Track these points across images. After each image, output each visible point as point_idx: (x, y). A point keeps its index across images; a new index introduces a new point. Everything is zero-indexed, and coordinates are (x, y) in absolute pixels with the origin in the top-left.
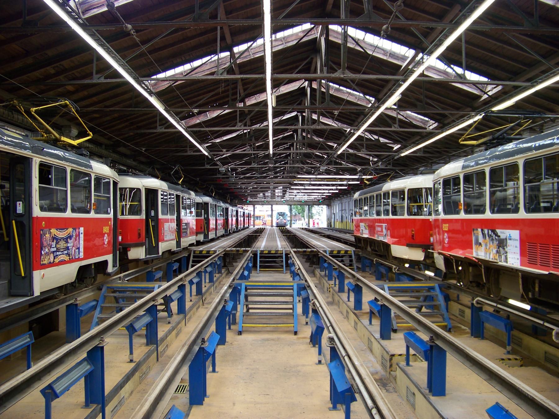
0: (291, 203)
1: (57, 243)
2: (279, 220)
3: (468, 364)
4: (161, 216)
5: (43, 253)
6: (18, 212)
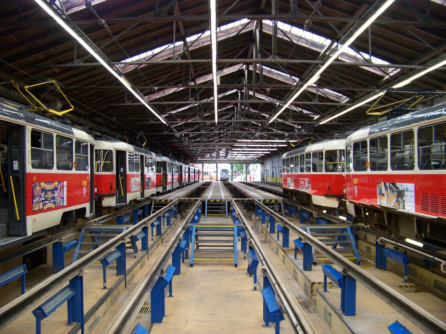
0: (232, 162)
1: (45, 194)
2: (223, 176)
3: (373, 290)
4: (128, 172)
5: (34, 201)
6: (14, 169)
